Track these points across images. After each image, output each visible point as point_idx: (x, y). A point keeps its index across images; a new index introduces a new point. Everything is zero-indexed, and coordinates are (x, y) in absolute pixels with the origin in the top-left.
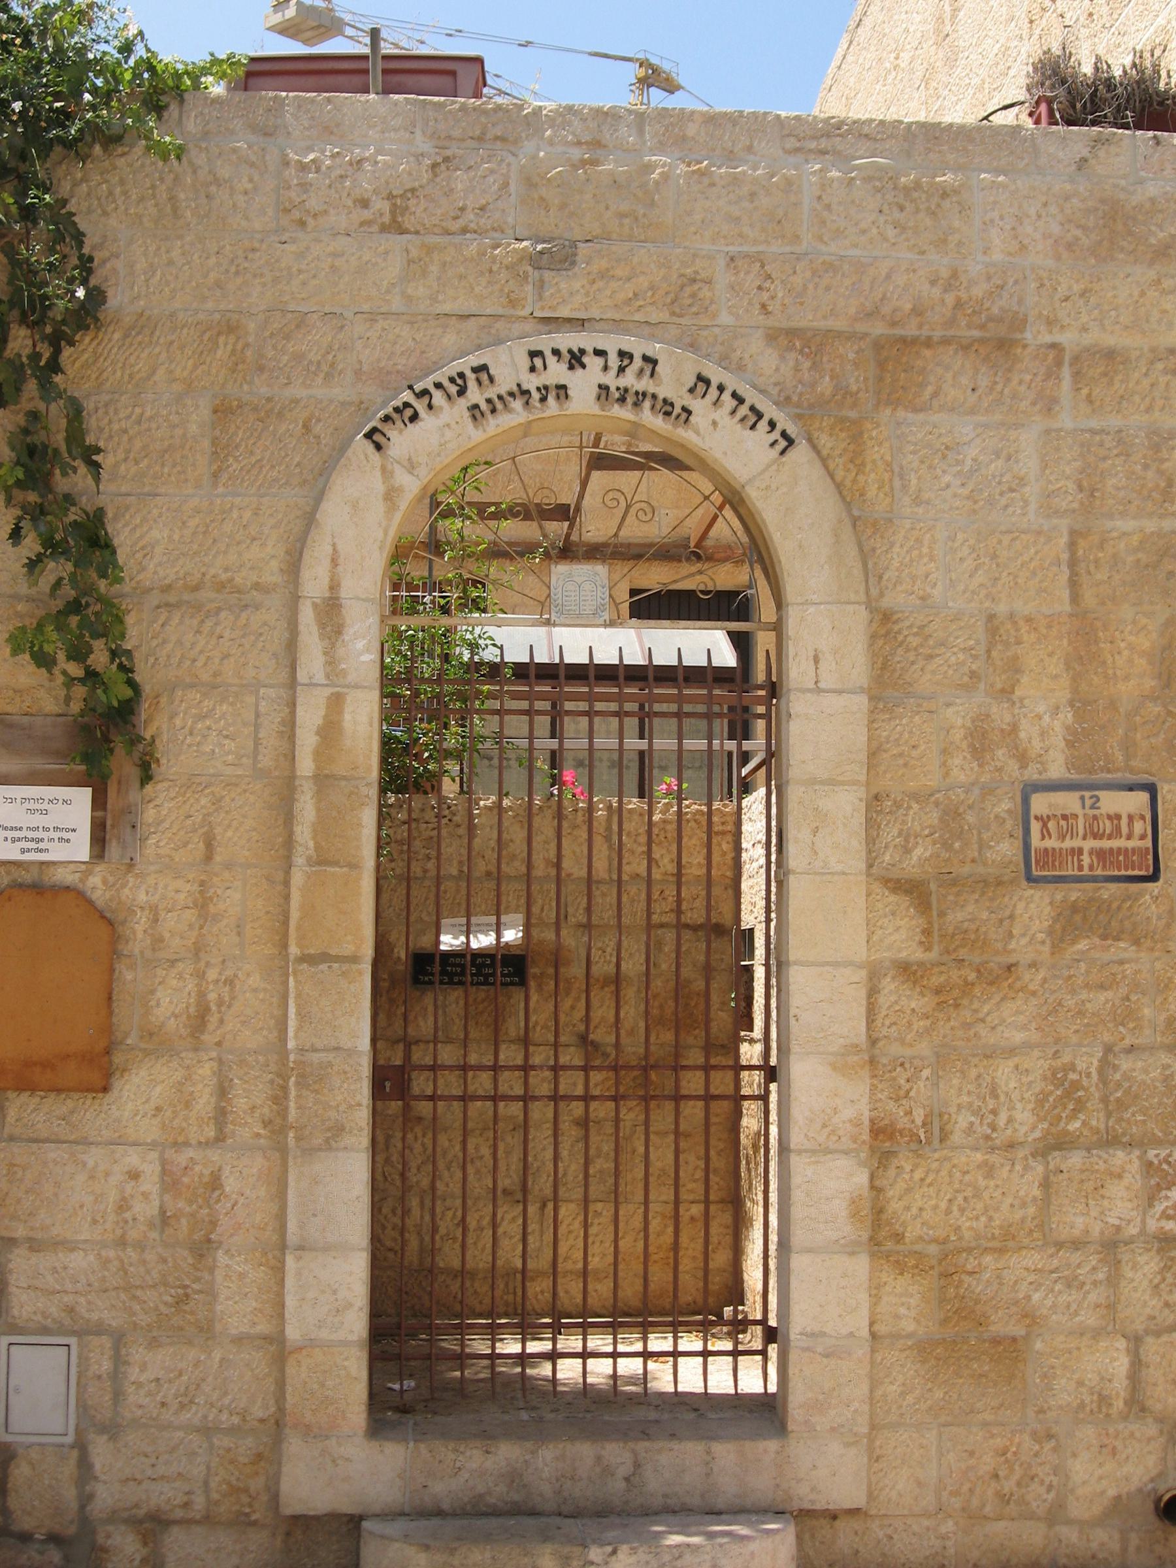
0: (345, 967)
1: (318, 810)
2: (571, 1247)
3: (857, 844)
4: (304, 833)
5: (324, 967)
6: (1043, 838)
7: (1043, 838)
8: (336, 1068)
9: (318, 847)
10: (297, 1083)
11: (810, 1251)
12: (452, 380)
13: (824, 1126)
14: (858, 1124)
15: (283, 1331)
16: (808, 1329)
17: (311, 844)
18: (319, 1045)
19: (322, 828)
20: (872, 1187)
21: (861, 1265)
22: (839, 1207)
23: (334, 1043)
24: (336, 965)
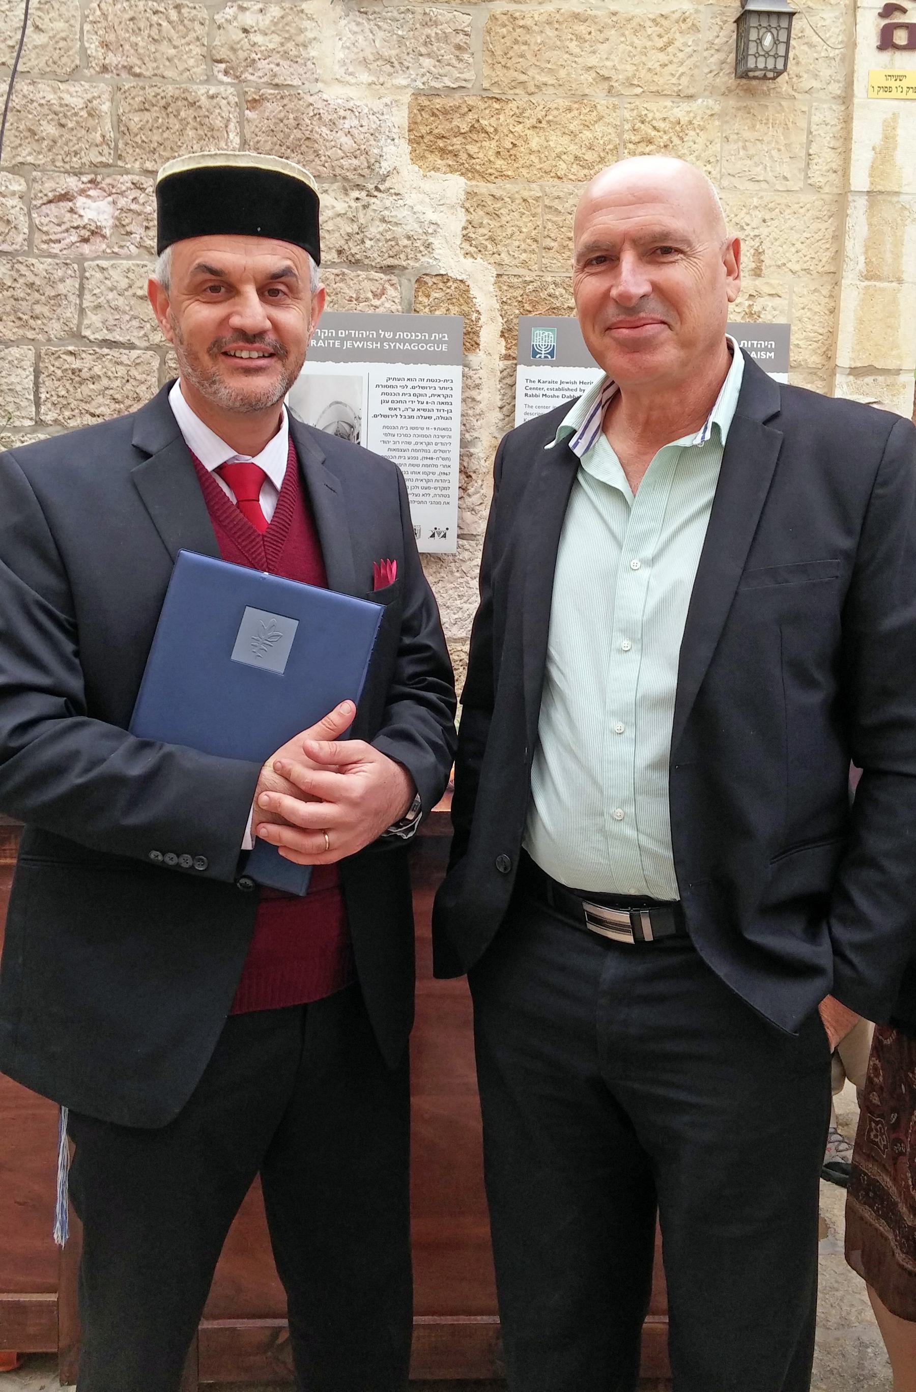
0: (890, 379)
1: (870, 225)
4: (854, 247)
5: (869, 379)
9: (868, 263)
17: (862, 259)
19: (872, 245)
24: (881, 379)
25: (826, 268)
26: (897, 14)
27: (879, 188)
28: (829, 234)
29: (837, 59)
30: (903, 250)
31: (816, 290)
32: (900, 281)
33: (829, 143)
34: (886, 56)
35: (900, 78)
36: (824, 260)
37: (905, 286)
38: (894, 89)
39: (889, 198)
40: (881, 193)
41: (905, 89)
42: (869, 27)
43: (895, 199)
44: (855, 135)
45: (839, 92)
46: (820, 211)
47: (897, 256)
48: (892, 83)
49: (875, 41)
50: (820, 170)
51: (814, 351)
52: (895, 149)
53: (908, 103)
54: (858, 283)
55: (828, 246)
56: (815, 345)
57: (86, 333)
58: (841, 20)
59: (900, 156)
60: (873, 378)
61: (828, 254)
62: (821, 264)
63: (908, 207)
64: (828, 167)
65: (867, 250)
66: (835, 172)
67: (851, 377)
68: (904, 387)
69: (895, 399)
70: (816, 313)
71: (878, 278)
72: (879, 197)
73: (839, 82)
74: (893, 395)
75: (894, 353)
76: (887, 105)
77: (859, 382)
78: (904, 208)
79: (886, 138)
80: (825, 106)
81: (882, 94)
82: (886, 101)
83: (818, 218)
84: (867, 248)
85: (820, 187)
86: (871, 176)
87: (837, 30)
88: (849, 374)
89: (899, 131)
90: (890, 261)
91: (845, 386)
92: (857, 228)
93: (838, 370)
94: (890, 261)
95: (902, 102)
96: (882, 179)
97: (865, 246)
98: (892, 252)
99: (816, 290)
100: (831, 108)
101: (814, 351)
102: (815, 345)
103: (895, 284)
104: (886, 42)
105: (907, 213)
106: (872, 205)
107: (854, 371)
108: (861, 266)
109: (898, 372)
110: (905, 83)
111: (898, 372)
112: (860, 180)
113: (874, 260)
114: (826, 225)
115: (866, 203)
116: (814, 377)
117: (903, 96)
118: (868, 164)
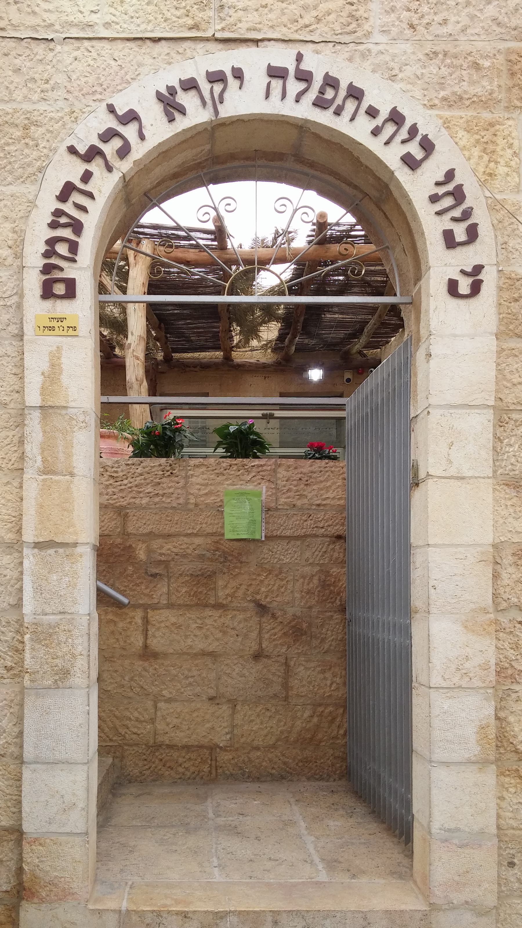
0: (69, 551)
1: (44, 432)
2: (175, 270)
3: (487, 455)
4: (33, 449)
5: (51, 551)
6: (171, 120)
7: (171, 120)
8: (62, 627)
9: (44, 461)
10: (32, 639)
11: (447, 764)
12: (54, 225)
13: (458, 669)
14: (485, 667)
15: (21, 825)
16: (446, 826)
17: (39, 458)
18: (48, 610)
19: (47, 447)
20: (497, 718)
21: (489, 777)
22: (470, 732)
23: (60, 609)
24: (61, 551)
25: (15, 466)
26: (56, 271)
27: (50, 403)
28: (16, 440)
29: (14, 307)
30: (74, 451)
31: (8, 483)
32: (72, 475)
33: (11, 370)
34: (48, 304)
35: (62, 320)
36: (14, 459)
37: (76, 479)
38: (57, 329)
39: (59, 412)
40: (52, 407)
41: (66, 328)
42: (33, 282)
43: (64, 412)
44: (27, 363)
45: (16, 332)
46: (8, 422)
47: (69, 456)
48: (54, 324)
49: (38, 291)
50: (5, 391)
51: (10, 530)
52: (61, 374)
53: (69, 338)
54: (37, 477)
55: (16, 449)
56: (10, 525)
57: (279, 507)
58: (15, 277)
59: (65, 379)
60: (54, 550)
61: (16, 455)
62: (11, 463)
63: (75, 418)
64: (11, 389)
65: (43, 451)
66: (17, 392)
67: (36, 550)
68: (81, 556)
69: (74, 566)
70: (9, 500)
71: (54, 473)
72: (51, 411)
73: (16, 324)
74: (73, 563)
75: (71, 530)
76: (51, 341)
77: (43, 554)
78: (71, 418)
79: (53, 365)
80: (6, 342)
81: (47, 332)
82: (50, 337)
83: (6, 428)
84: (43, 450)
85: (6, 404)
86: (42, 394)
87: (12, 285)
88: (34, 547)
89: (63, 360)
90: (63, 459)
91: (31, 557)
92: (34, 435)
93: (25, 544)
94: (63, 459)
95: (64, 339)
96: (51, 397)
97: (41, 448)
98: (64, 453)
99: (8, 483)
100: (11, 344)
101: (10, 530)
102: (10, 525)
103: (68, 477)
104: (47, 293)
105: (74, 422)
106: (45, 418)
107: (38, 545)
108: (39, 462)
109: (75, 545)
110: (65, 324)
111: (75, 545)
112: (33, 398)
113: (49, 458)
114: (13, 433)
115: (39, 415)
116: (12, 550)
117: (65, 333)
118: (39, 386)
